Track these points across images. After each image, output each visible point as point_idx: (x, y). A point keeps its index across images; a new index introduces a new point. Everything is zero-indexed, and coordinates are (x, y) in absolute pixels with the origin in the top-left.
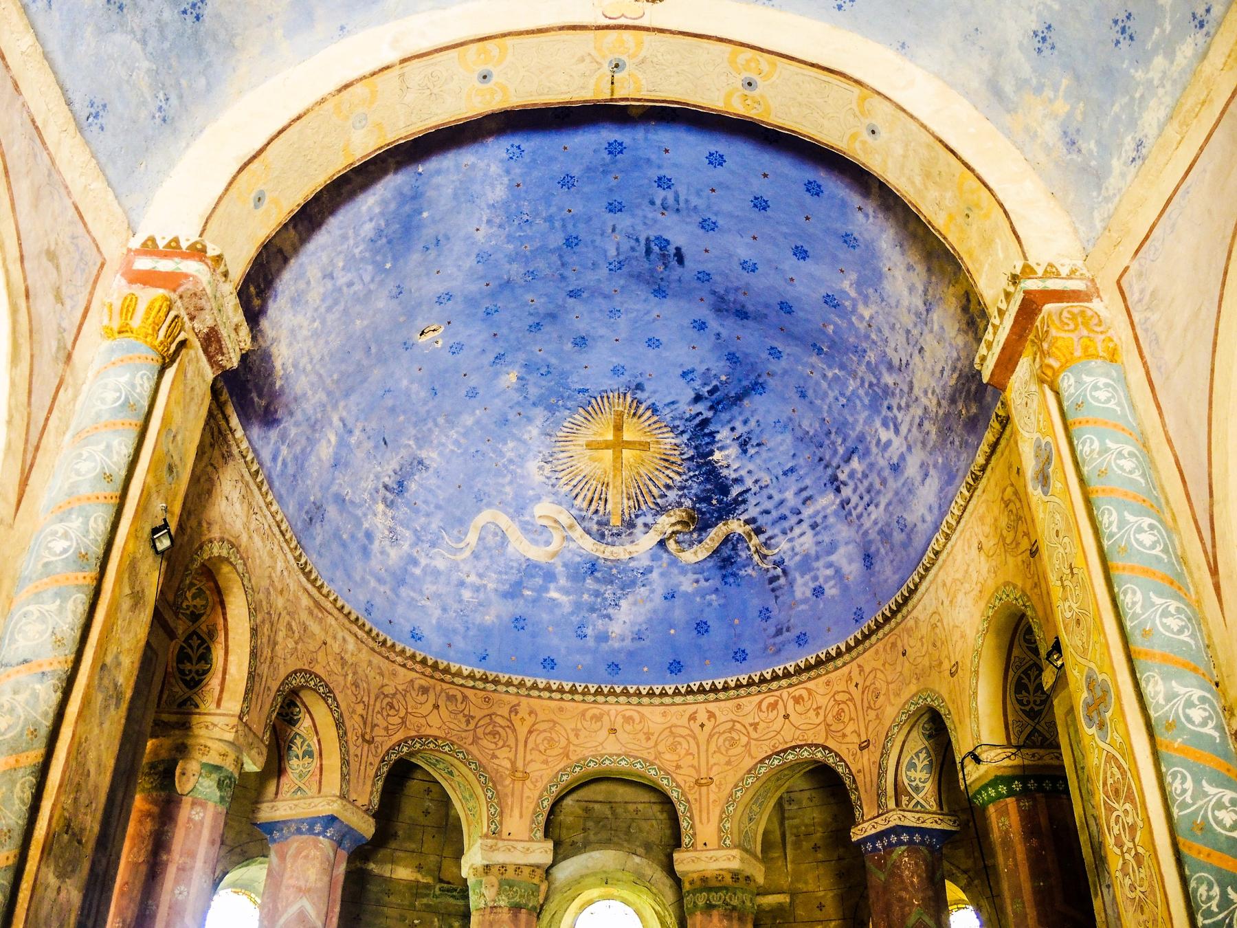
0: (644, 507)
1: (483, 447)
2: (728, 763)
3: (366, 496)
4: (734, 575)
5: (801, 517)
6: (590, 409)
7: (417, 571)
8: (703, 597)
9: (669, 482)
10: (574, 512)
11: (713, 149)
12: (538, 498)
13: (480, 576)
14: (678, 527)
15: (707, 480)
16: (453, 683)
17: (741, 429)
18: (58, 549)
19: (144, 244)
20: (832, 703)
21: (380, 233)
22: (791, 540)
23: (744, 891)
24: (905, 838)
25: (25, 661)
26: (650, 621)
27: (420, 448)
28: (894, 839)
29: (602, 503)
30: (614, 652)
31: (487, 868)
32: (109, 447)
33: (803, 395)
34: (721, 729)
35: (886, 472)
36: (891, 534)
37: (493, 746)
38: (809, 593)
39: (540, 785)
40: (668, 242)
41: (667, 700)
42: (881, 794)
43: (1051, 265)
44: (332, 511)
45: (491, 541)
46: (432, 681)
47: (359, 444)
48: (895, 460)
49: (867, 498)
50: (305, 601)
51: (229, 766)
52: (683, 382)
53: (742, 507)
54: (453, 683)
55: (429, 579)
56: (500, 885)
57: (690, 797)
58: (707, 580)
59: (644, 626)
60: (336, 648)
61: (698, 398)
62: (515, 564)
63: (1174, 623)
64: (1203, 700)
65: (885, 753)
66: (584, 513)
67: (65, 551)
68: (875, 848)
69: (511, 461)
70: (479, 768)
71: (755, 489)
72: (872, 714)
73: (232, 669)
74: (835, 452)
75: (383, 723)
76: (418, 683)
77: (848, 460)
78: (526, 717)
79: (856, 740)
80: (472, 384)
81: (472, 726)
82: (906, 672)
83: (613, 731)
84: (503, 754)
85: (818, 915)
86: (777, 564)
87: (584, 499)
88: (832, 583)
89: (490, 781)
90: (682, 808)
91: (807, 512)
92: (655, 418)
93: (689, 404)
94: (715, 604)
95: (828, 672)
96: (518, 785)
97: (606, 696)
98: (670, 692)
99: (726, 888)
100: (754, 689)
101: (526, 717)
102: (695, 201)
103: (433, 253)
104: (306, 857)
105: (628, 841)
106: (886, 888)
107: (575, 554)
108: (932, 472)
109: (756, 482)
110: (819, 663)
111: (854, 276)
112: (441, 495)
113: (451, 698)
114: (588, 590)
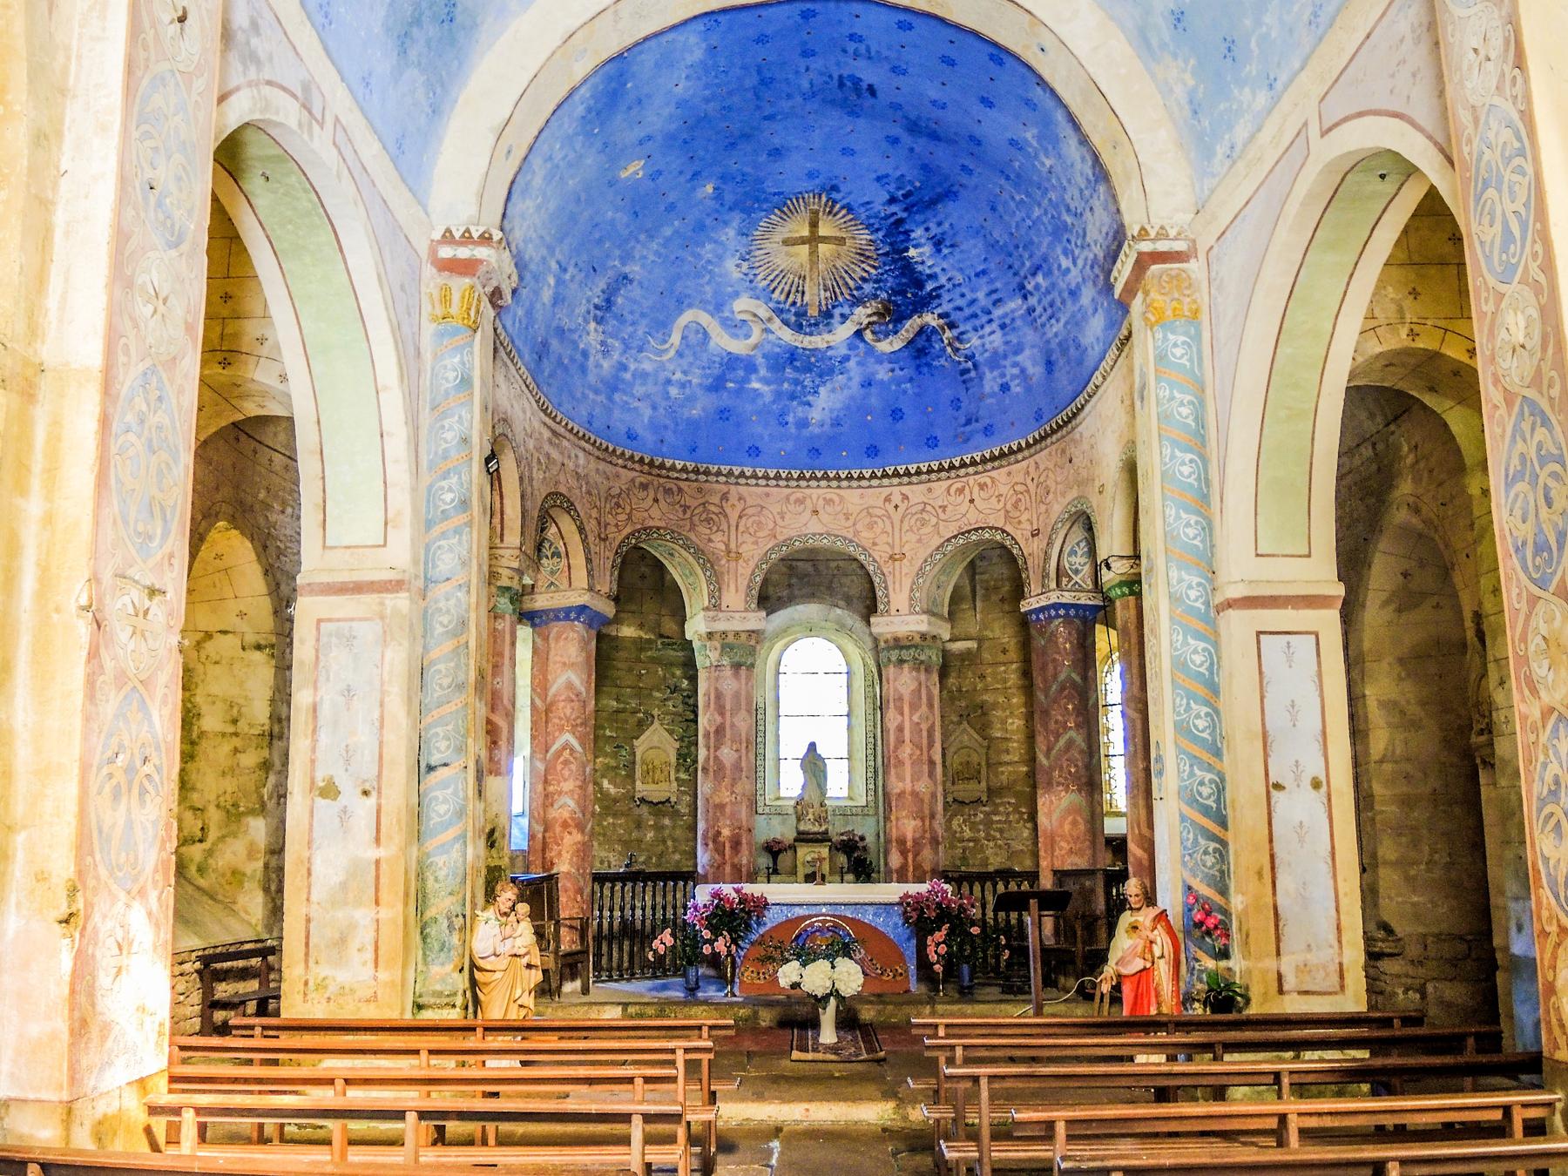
0: (840, 299)
1: (680, 253)
2: (919, 541)
3: (580, 320)
4: (928, 365)
5: (992, 316)
6: (785, 209)
7: (628, 376)
8: (898, 385)
9: (865, 275)
10: (772, 305)
11: (902, 18)
12: (736, 295)
13: (685, 373)
14: (875, 318)
15: (903, 275)
16: (668, 477)
17: (935, 230)
18: (448, 500)
19: (444, 236)
20: (1012, 492)
21: (589, 110)
22: (981, 337)
23: (930, 647)
24: (1062, 612)
25: (448, 579)
26: (848, 408)
27: (624, 264)
28: (1053, 613)
29: (799, 295)
30: (812, 437)
31: (710, 635)
32: (460, 417)
33: (993, 209)
34: (913, 510)
35: (1066, 295)
36: (1068, 349)
37: (708, 531)
38: (996, 389)
39: (752, 564)
40: (861, 80)
41: (864, 483)
42: (1045, 576)
43: (1162, 228)
44: (555, 344)
45: (693, 339)
46: (650, 478)
47: (573, 278)
48: (1073, 286)
49: (1049, 311)
50: (547, 434)
51: (515, 585)
52: (877, 185)
53: (936, 302)
54: (668, 477)
55: (638, 381)
56: (723, 647)
57: (885, 571)
58: (902, 369)
59: (841, 414)
60: (571, 465)
61: (892, 200)
62: (717, 359)
63: (1191, 532)
64: (1199, 584)
65: (1050, 544)
66: (781, 306)
67: (453, 501)
68: (1038, 618)
69: (709, 262)
70: (698, 553)
71: (949, 286)
72: (1043, 508)
73: (508, 510)
74: (1023, 264)
75: (613, 522)
76: (638, 481)
77: (1034, 274)
78: (736, 503)
79: (1029, 527)
80: (671, 200)
81: (688, 515)
82: (1071, 478)
83: (816, 512)
84: (717, 537)
85: (1002, 658)
86: (969, 358)
87: (781, 292)
88: (1017, 381)
89: (708, 562)
90: (878, 580)
91: (998, 312)
92: (851, 216)
93: (884, 205)
94: (910, 392)
95: (1009, 464)
96: (733, 564)
97: (808, 480)
98: (867, 476)
99: (916, 647)
100: (943, 474)
101: (736, 503)
102: (885, 53)
103: (634, 112)
104: (566, 639)
105: (831, 596)
106: (1044, 653)
107: (774, 345)
108: (1100, 310)
109: (950, 279)
110: (1002, 455)
111: (1035, 131)
112: (646, 304)
113: (668, 491)
114: (788, 380)
